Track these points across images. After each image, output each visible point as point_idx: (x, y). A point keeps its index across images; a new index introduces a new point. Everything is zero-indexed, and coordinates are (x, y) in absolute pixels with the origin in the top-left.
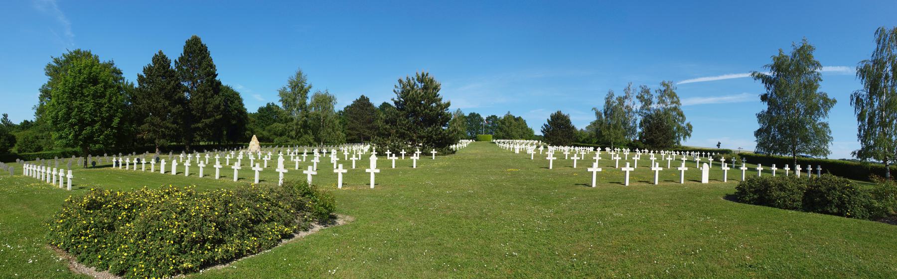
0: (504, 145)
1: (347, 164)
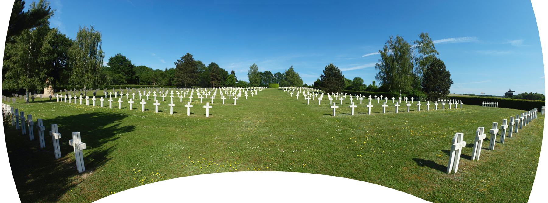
1: (338, 103)
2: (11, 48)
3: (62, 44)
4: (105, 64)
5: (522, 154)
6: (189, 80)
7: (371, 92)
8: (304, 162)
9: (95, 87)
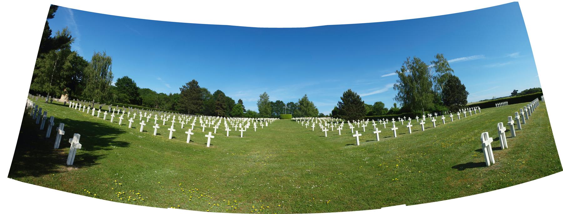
2: (41, 62)
3: (80, 64)
4: (113, 83)
5: (538, 132)
6: (193, 107)
7: (394, 114)
8: (328, 198)
9: (102, 102)
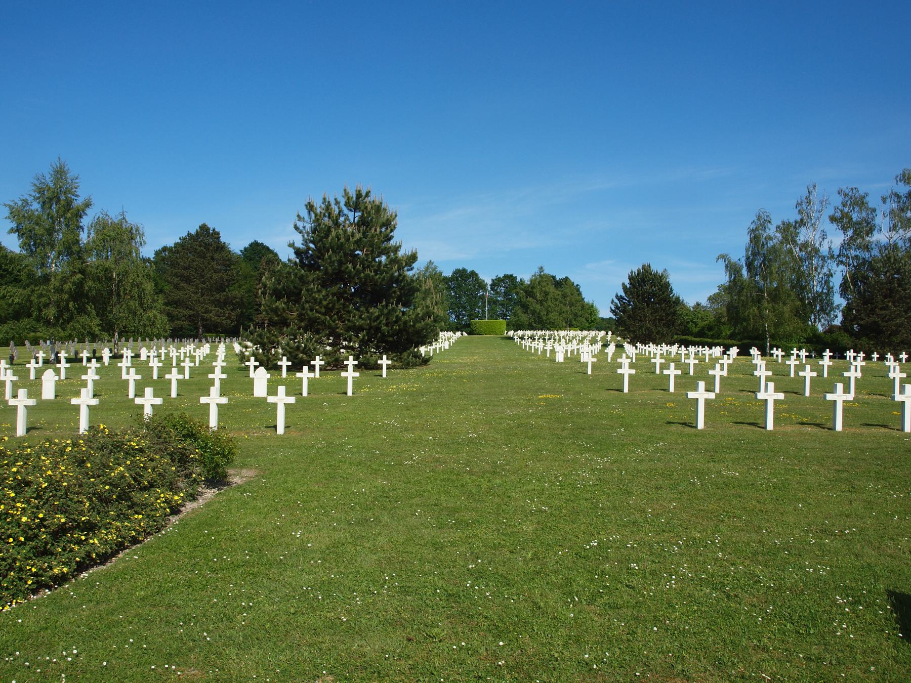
0: (534, 342)
